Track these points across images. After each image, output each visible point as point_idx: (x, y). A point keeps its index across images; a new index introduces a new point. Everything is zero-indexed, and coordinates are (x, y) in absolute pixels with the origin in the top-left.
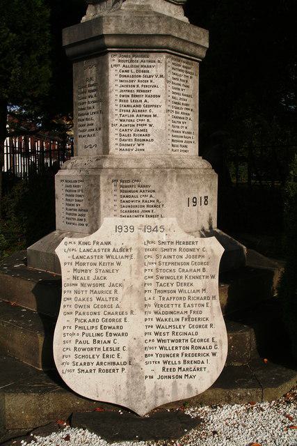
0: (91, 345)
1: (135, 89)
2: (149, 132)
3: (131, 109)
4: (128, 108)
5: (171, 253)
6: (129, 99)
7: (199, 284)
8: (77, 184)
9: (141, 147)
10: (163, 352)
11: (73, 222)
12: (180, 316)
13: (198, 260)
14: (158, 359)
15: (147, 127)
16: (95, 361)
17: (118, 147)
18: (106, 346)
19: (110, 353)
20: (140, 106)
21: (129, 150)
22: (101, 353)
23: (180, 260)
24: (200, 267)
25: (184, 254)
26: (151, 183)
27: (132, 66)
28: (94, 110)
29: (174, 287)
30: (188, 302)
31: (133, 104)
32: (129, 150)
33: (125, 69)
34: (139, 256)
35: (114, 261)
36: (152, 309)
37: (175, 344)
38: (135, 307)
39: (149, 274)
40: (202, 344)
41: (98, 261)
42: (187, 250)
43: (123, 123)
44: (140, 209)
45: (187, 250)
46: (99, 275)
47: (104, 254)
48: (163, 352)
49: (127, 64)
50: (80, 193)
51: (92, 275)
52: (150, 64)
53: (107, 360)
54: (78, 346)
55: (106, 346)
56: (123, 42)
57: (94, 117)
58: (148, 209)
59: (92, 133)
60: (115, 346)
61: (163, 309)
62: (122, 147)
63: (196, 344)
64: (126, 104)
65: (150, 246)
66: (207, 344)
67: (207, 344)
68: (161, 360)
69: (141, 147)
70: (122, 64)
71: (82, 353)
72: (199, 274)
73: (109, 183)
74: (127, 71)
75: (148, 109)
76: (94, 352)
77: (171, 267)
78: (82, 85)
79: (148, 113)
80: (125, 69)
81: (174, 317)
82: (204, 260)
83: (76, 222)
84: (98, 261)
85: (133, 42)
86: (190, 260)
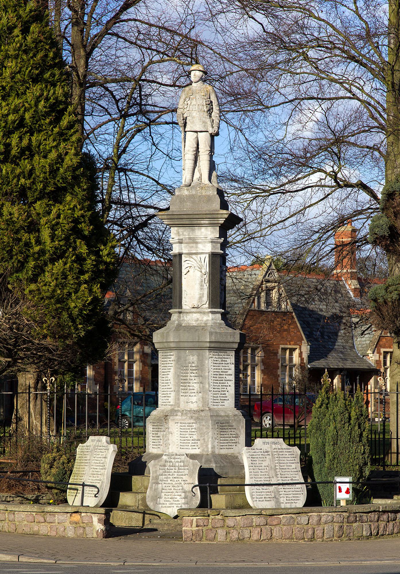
0: (261, 491)
1: (220, 371)
2: (227, 395)
3: (219, 382)
4: (217, 382)
5: (283, 453)
6: (217, 376)
7: (294, 466)
8: (191, 425)
9: (223, 404)
10: (285, 493)
11: (187, 447)
12: (289, 479)
13: (292, 456)
14: (284, 496)
15: (226, 392)
16: (263, 497)
17: (212, 403)
18: (266, 491)
19: (268, 494)
20: (222, 380)
21: (217, 405)
22: (265, 494)
23: (286, 456)
24: (293, 459)
25: (287, 454)
26: (234, 424)
27: (219, 358)
28: (195, 381)
29: (286, 467)
30: (291, 473)
31: (219, 379)
32: (217, 405)
33: (215, 359)
34: (272, 455)
35: (264, 457)
36: (279, 476)
37: (289, 490)
38: (274, 475)
39: (277, 462)
40: (298, 490)
41: (259, 457)
42: (288, 452)
43: (215, 390)
44: (229, 439)
45: (288, 452)
46: (260, 462)
47: (260, 454)
48: (285, 493)
49: (217, 357)
50: (194, 430)
51: (258, 462)
52: (227, 357)
53: (268, 496)
54: (257, 491)
55: (266, 491)
56: (216, 345)
57: (195, 385)
58: (233, 439)
59: (194, 394)
60: (269, 491)
61: (283, 476)
62: (214, 404)
63: (296, 490)
64: (216, 379)
65: (275, 450)
66: (300, 490)
67: (300, 490)
68: (285, 496)
69: (223, 404)
70: (214, 357)
71: (258, 494)
72: (293, 462)
73: (214, 425)
74: (217, 361)
75: (226, 382)
76: (263, 493)
77: (284, 459)
78: (185, 365)
79: (226, 384)
80: (215, 359)
81: (287, 479)
82: (294, 456)
83: (189, 447)
84: (259, 457)
85: (222, 345)
86: (289, 456)
